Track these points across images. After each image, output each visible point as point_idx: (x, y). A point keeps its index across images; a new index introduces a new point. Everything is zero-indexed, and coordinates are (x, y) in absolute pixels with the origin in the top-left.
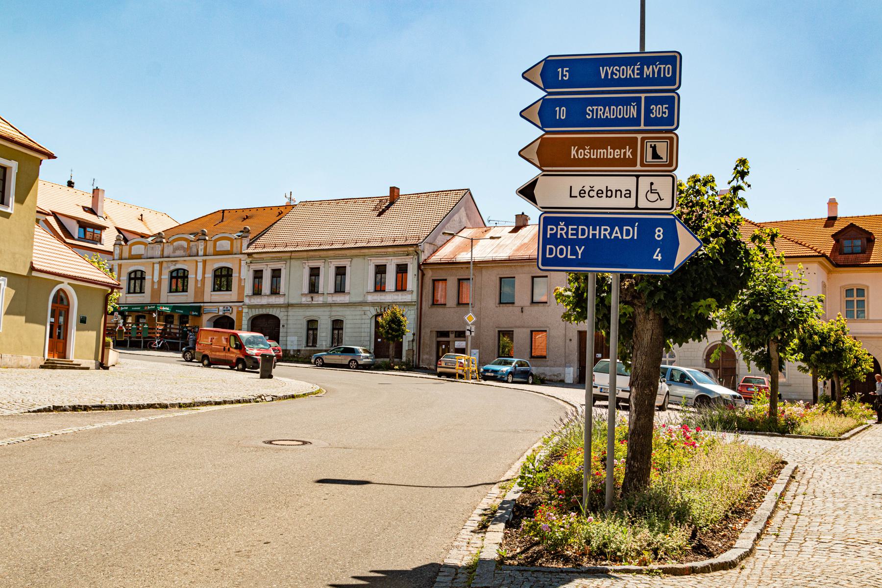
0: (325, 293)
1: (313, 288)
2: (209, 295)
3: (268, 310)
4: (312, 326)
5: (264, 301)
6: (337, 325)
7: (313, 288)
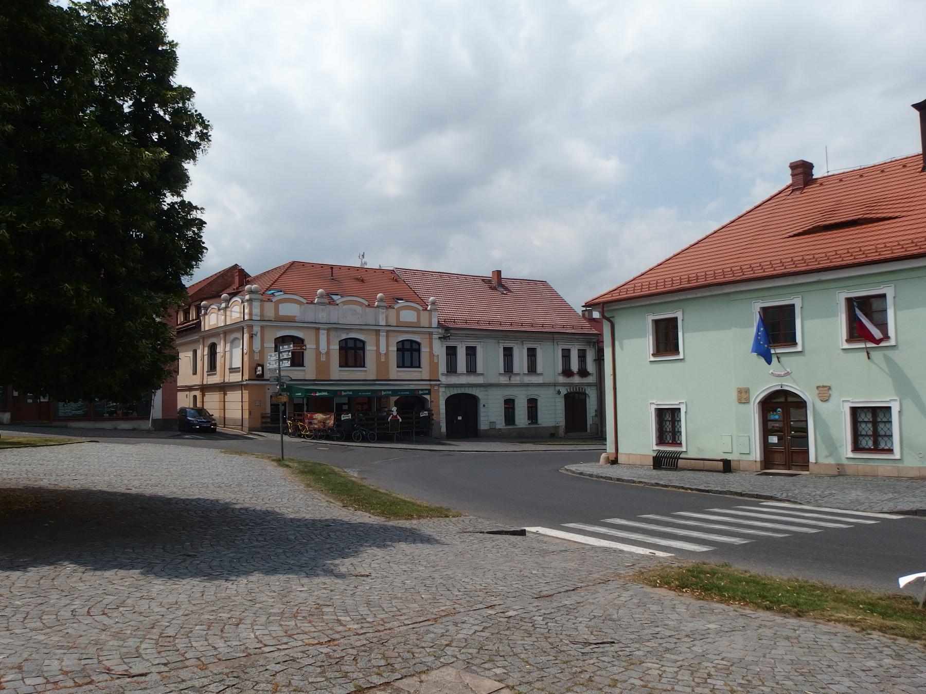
0: (521, 373)
1: (509, 368)
2: (395, 372)
3: (467, 389)
4: (509, 404)
5: (463, 380)
6: (532, 404)
7: (509, 368)
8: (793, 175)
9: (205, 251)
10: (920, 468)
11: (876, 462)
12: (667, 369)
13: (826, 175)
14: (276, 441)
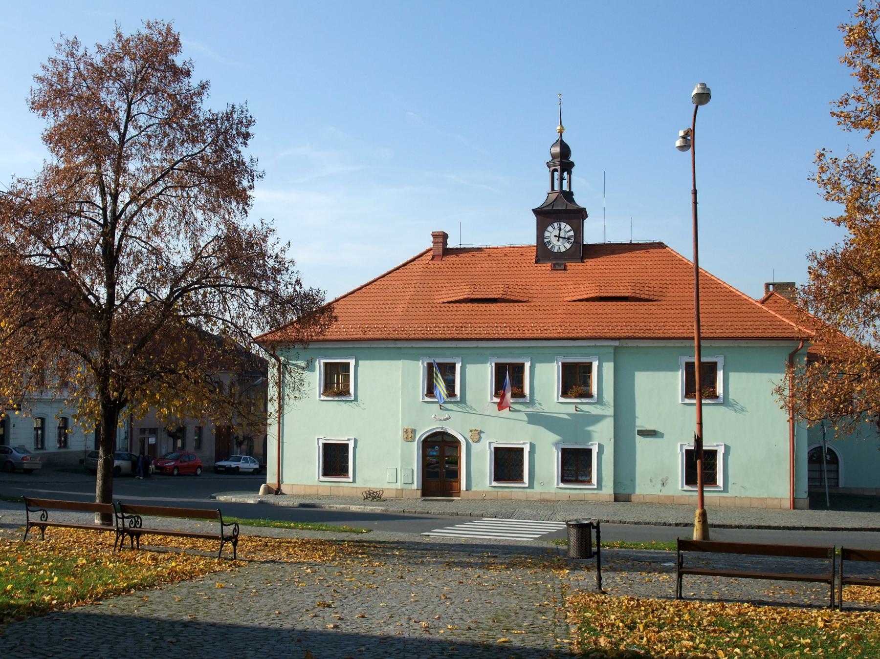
8: (434, 243)
9: (41, 112)
10: (541, 493)
11: (511, 490)
12: (335, 407)
13: (459, 247)
14: (228, 515)
